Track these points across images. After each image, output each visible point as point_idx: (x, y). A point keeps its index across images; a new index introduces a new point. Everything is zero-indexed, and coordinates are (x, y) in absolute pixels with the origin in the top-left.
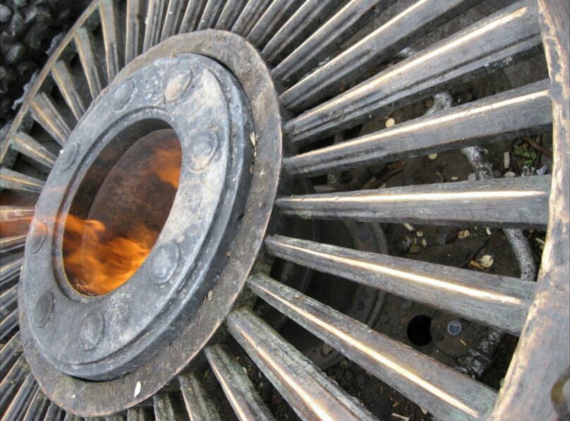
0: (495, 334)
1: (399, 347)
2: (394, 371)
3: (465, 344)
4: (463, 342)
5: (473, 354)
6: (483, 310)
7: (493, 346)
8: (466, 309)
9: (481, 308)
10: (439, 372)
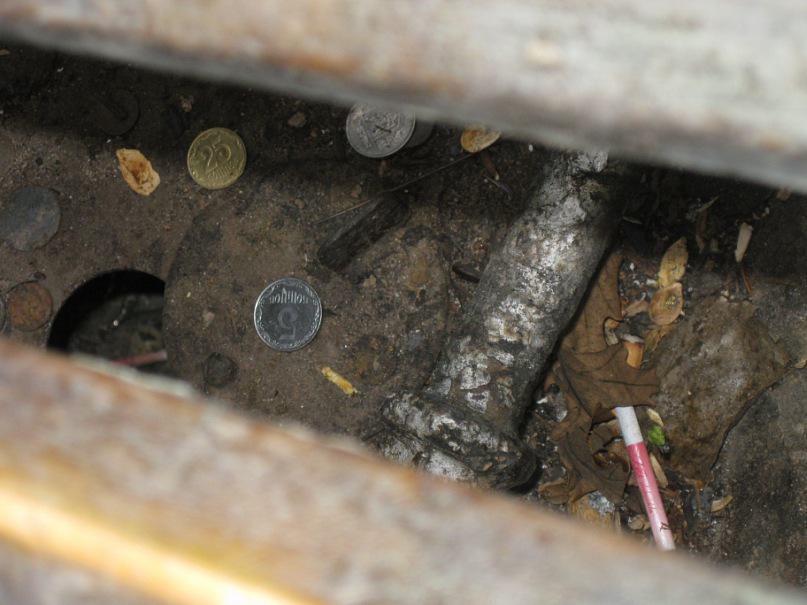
0: (517, 308)
1: (102, 398)
2: (94, 572)
3: (350, 390)
4: (335, 378)
5: (418, 423)
6: (698, 43)
7: (511, 371)
8: (574, 53)
9: (692, 25)
10: (426, 538)
